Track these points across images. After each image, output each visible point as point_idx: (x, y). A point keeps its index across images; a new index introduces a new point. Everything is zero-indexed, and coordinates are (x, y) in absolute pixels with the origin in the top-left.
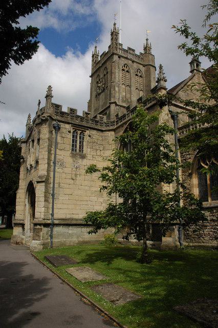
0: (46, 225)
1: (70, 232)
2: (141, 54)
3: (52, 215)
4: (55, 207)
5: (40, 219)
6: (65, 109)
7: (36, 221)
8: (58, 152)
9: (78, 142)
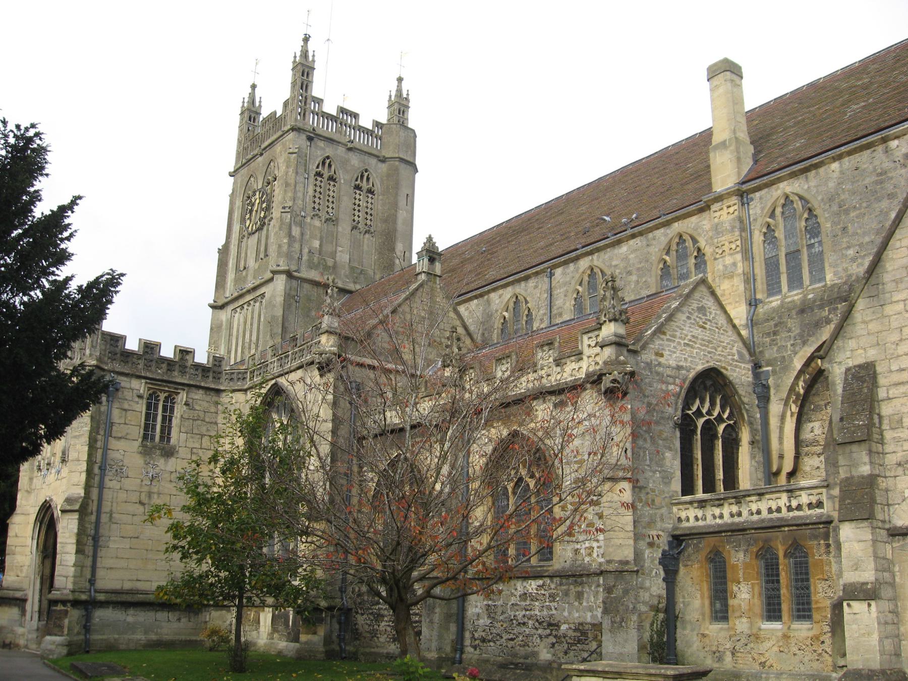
0: (76, 603)
1: (130, 619)
2: (377, 124)
3: (92, 581)
4: (98, 565)
5: (65, 592)
6: (132, 345)
7: (55, 595)
8: (113, 444)
9: (159, 418)
